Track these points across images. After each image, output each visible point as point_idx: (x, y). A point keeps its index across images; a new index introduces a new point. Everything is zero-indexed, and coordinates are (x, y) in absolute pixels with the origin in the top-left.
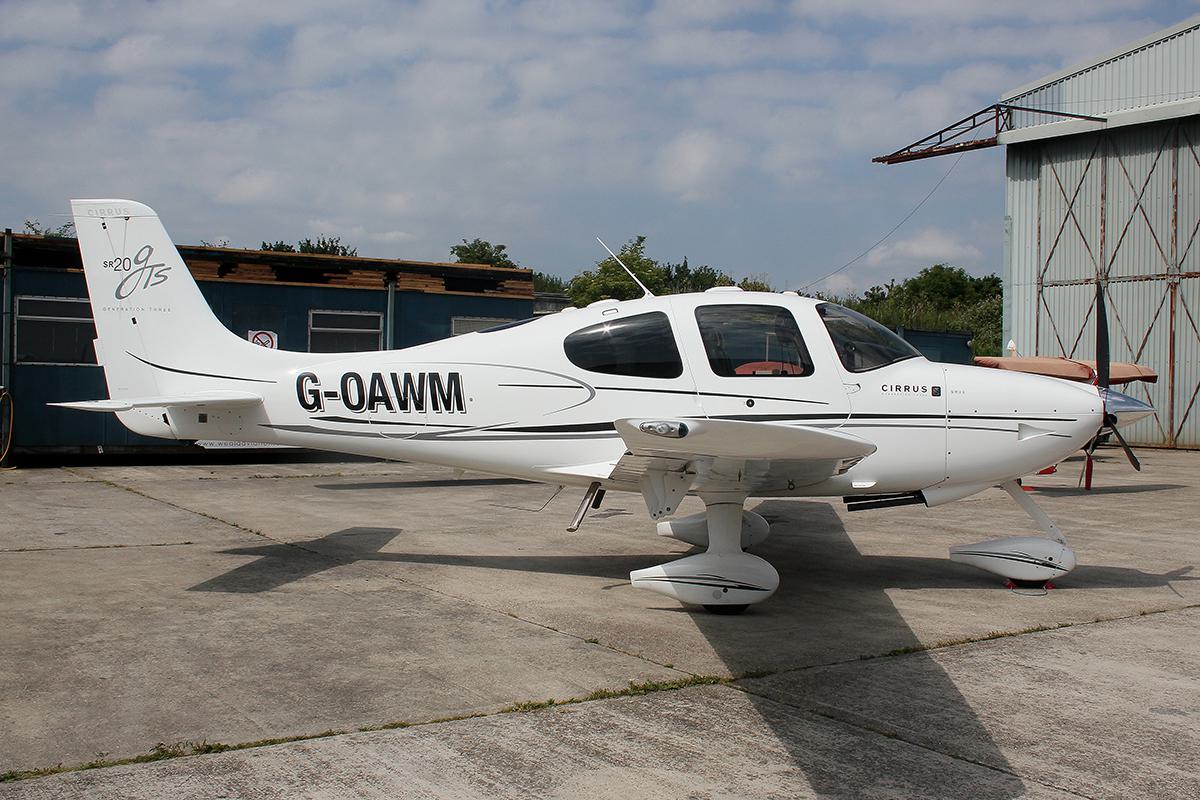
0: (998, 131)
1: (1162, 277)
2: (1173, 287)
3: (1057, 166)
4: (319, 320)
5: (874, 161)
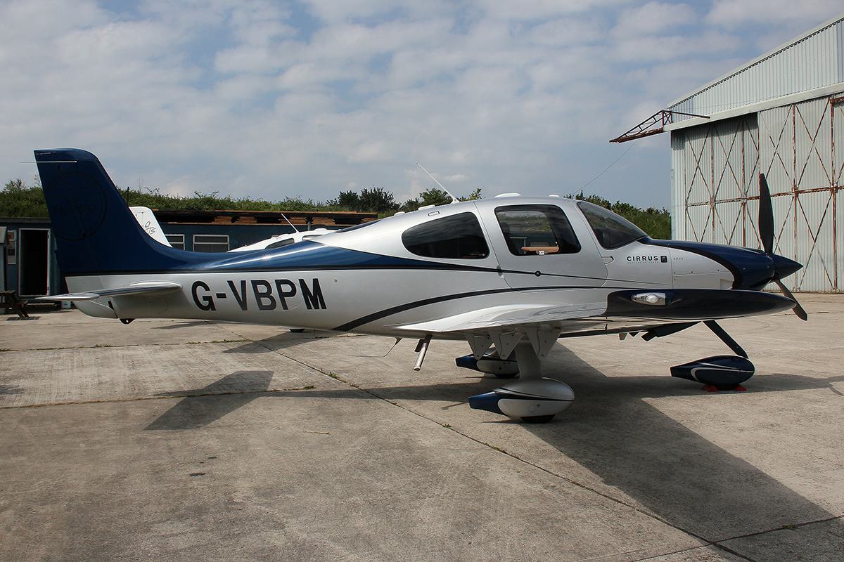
0: (664, 125)
1: (738, 200)
2: (744, 204)
3: (721, 137)
4: (197, 239)
5: (610, 141)
